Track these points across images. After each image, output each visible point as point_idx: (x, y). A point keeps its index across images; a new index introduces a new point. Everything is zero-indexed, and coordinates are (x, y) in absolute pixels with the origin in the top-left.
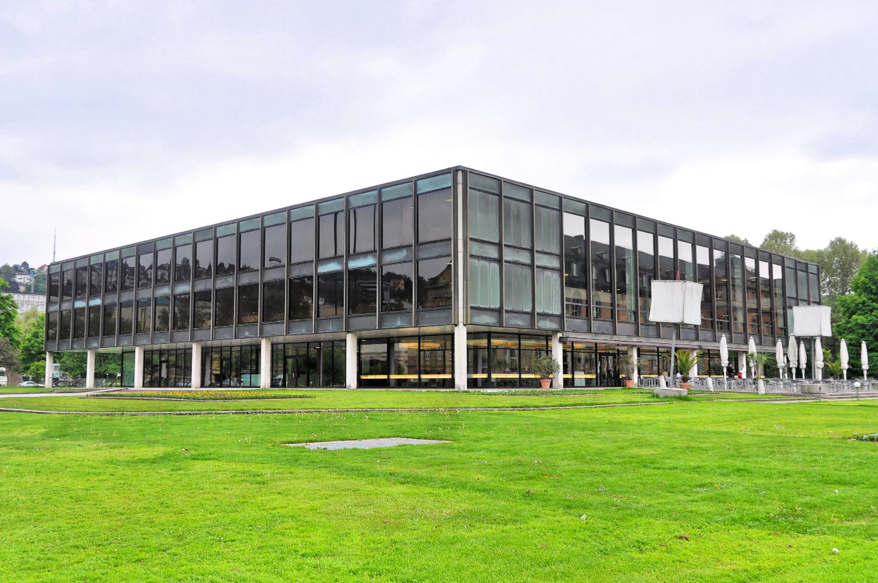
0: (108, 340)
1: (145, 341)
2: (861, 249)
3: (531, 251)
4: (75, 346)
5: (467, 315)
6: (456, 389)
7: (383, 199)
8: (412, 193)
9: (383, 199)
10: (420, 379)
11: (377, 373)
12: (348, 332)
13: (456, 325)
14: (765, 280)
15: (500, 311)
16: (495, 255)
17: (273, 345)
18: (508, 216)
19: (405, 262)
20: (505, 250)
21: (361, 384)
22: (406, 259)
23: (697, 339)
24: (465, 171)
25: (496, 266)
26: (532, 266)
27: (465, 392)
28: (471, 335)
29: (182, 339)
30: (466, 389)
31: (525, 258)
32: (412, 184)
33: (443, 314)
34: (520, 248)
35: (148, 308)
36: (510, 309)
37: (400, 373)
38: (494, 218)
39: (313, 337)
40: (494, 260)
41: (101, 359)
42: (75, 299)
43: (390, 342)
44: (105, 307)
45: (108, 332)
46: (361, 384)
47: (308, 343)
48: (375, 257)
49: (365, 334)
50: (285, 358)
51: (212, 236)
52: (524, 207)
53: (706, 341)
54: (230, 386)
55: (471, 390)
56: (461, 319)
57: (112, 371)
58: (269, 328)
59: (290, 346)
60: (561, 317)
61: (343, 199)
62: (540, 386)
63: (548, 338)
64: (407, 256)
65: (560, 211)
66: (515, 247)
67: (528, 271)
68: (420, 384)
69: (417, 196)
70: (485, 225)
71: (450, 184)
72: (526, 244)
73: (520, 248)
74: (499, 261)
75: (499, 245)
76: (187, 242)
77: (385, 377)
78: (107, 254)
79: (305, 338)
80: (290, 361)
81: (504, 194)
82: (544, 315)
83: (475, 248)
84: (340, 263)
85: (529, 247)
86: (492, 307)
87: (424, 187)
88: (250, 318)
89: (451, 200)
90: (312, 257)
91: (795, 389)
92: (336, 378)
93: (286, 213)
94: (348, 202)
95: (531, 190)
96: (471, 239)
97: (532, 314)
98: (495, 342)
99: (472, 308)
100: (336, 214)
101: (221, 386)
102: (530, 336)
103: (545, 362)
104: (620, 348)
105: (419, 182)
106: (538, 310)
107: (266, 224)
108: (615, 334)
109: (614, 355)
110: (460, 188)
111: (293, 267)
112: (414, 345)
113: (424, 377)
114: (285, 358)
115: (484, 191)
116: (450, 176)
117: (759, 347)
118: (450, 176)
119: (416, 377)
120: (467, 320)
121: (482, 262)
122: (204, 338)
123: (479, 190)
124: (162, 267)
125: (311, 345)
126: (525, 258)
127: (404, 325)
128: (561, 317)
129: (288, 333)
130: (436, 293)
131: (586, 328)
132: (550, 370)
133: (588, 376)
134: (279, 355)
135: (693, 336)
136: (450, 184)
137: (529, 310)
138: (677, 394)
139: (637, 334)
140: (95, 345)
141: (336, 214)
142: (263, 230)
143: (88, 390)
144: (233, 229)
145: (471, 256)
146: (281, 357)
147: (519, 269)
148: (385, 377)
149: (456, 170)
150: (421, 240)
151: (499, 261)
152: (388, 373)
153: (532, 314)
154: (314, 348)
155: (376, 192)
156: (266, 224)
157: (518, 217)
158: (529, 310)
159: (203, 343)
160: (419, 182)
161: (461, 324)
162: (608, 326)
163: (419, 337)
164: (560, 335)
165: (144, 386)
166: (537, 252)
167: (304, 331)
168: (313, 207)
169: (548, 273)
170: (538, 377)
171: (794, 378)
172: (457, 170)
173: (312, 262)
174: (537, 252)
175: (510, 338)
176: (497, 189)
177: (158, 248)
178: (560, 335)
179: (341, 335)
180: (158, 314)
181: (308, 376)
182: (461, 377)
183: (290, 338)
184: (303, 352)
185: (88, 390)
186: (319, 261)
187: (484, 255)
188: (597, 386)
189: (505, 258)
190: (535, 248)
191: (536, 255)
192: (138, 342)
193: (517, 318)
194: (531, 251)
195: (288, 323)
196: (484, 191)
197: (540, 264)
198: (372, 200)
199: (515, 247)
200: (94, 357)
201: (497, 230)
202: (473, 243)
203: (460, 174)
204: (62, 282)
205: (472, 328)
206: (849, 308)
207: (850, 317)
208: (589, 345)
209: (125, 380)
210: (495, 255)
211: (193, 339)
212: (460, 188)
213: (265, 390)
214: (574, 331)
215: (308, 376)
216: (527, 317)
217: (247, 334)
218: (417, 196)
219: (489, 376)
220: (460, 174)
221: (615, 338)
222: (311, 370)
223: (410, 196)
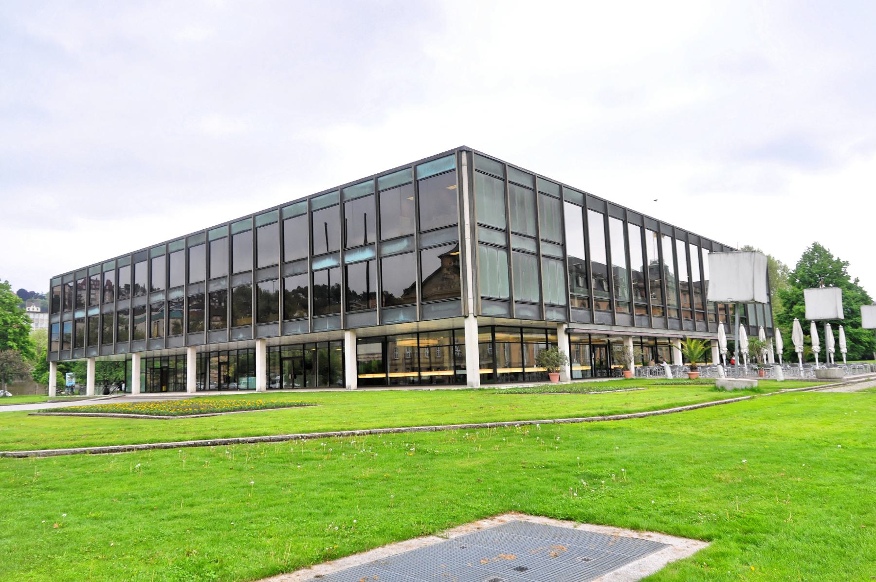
0: (106, 349)
1: (140, 347)
3: (536, 239)
4: (76, 355)
5: (477, 306)
6: (468, 387)
7: (380, 189)
8: (412, 179)
10: (420, 376)
11: (377, 374)
12: (346, 330)
13: (466, 317)
14: (683, 284)
15: (509, 301)
16: (503, 243)
17: (269, 348)
18: (513, 201)
19: (406, 253)
20: (512, 237)
21: (362, 383)
22: (408, 249)
23: (681, 329)
24: (469, 152)
25: (503, 254)
26: (537, 254)
27: (480, 389)
28: (482, 329)
29: (177, 344)
30: (479, 386)
31: (530, 246)
32: (412, 170)
33: (452, 306)
34: (524, 236)
35: (161, 320)
36: (518, 299)
37: (396, 371)
38: (500, 204)
39: (309, 337)
40: (501, 247)
41: (100, 367)
42: (63, 313)
43: (385, 341)
44: (102, 315)
45: (106, 339)
46: (362, 383)
47: (304, 344)
48: (373, 249)
49: (361, 332)
50: (282, 360)
51: (205, 240)
52: (528, 194)
53: (688, 330)
54: (237, 389)
55: (486, 387)
56: (471, 310)
57: (113, 379)
58: (263, 329)
59: (287, 348)
60: (566, 308)
61: (338, 193)
62: (548, 379)
63: (554, 332)
64: (408, 246)
65: (561, 199)
66: (520, 235)
67: (534, 260)
68: (421, 382)
69: (417, 182)
70: (491, 210)
71: (454, 166)
72: (531, 232)
73: (524, 236)
74: (507, 248)
75: (506, 232)
77: (383, 376)
79: (299, 339)
80: (286, 363)
81: (508, 179)
82: (551, 306)
83: (483, 235)
84: (337, 258)
85: (533, 235)
86: (502, 297)
87: (424, 172)
88: (243, 321)
89: (456, 186)
90: (307, 254)
91: (812, 375)
92: (331, 376)
93: (278, 211)
94: (342, 195)
95: (534, 177)
96: (479, 225)
97: (540, 304)
98: (498, 336)
99: (482, 298)
102: (538, 329)
103: (554, 355)
104: (612, 340)
105: (418, 167)
106: (545, 301)
108: (614, 323)
109: (605, 346)
110: (465, 170)
111: (286, 266)
112: (411, 342)
113: (425, 374)
114: (282, 360)
115: (490, 175)
116: (454, 158)
117: (729, 335)
118: (454, 158)
119: (416, 374)
120: (478, 312)
121: (490, 249)
122: (198, 342)
123: (484, 173)
124: (301, 374)
125: (307, 346)
126: (530, 246)
127: (407, 319)
128: (566, 308)
129: (283, 334)
130: (443, 285)
131: (588, 319)
132: (556, 362)
133: (584, 368)
134: (274, 359)
135: (678, 326)
136: (454, 166)
137: (537, 300)
138: (749, 386)
139: (633, 324)
140: (94, 353)
142: (255, 230)
143: (89, 398)
144: (225, 231)
145: (480, 242)
146: (278, 360)
147: (526, 257)
148: (383, 376)
149: (461, 150)
150: (423, 229)
151: (507, 248)
152: (384, 371)
153: (540, 304)
154: (309, 350)
155: (372, 182)
156: (258, 224)
157: (522, 203)
158: (537, 300)
159: (198, 348)
160: (418, 167)
161: (471, 317)
162: (607, 317)
163: (418, 334)
164: (565, 326)
165: (141, 392)
166: (543, 240)
167: (299, 331)
168: (306, 203)
169: (552, 262)
171: (833, 362)
172: (461, 151)
173: (306, 259)
174: (543, 240)
175: (511, 333)
176: (502, 172)
178: (565, 326)
179: (336, 335)
180: (171, 326)
181: (305, 376)
182: (473, 371)
183: (285, 340)
184: (299, 353)
185: (89, 398)
186: (313, 257)
187: (493, 242)
188: (592, 377)
189: (512, 246)
190: (540, 237)
191: (541, 243)
192: (135, 349)
193: (526, 309)
194: (536, 239)
195: (283, 323)
196: (490, 175)
197: (545, 253)
198: (367, 191)
199: (520, 235)
200: (94, 365)
201: (503, 216)
202: (481, 228)
203: (464, 155)
204: (67, 294)
205: (487, 321)
206: (789, 300)
207: (791, 307)
208: (583, 337)
209: (123, 384)
210: (503, 243)
211: (187, 344)
212: (465, 170)
213: (261, 394)
214: (578, 322)
215: (305, 376)
216: (535, 308)
217: (241, 336)
218: (417, 182)
219: (495, 371)
220: (464, 155)
221: (614, 328)
222: (308, 371)
223: (411, 183)
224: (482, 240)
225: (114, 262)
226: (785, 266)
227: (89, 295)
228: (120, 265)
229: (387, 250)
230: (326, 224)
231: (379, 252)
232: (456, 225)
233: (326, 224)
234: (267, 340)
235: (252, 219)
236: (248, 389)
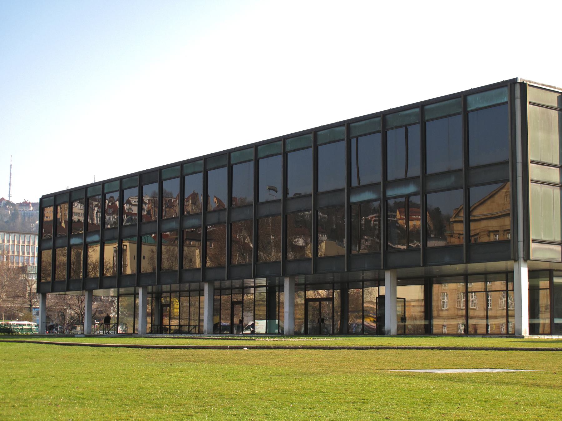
2: (442, 213)
8: (461, 110)
9: (427, 118)
24: (523, 86)
71: (506, 99)
76: (196, 170)
78: (106, 185)
87: (474, 103)
100: (406, 127)
101: (107, 335)
107: (289, 148)
110: (518, 102)
116: (506, 90)
118: (506, 90)
141: (406, 127)
147: (549, 188)
149: (514, 82)
150: (472, 163)
155: (417, 110)
170: (524, 271)
177: (164, 177)
212: (518, 102)
223: (379, 132)
224: (535, 179)
225: (118, 182)
226: (437, 210)
227: (55, 212)
228: (124, 187)
229: (432, 185)
230: (11, 165)
231: (424, 186)
232: (506, 163)
233: (11, 165)
234: (399, 270)
235: (281, 143)
236: (508, 335)
